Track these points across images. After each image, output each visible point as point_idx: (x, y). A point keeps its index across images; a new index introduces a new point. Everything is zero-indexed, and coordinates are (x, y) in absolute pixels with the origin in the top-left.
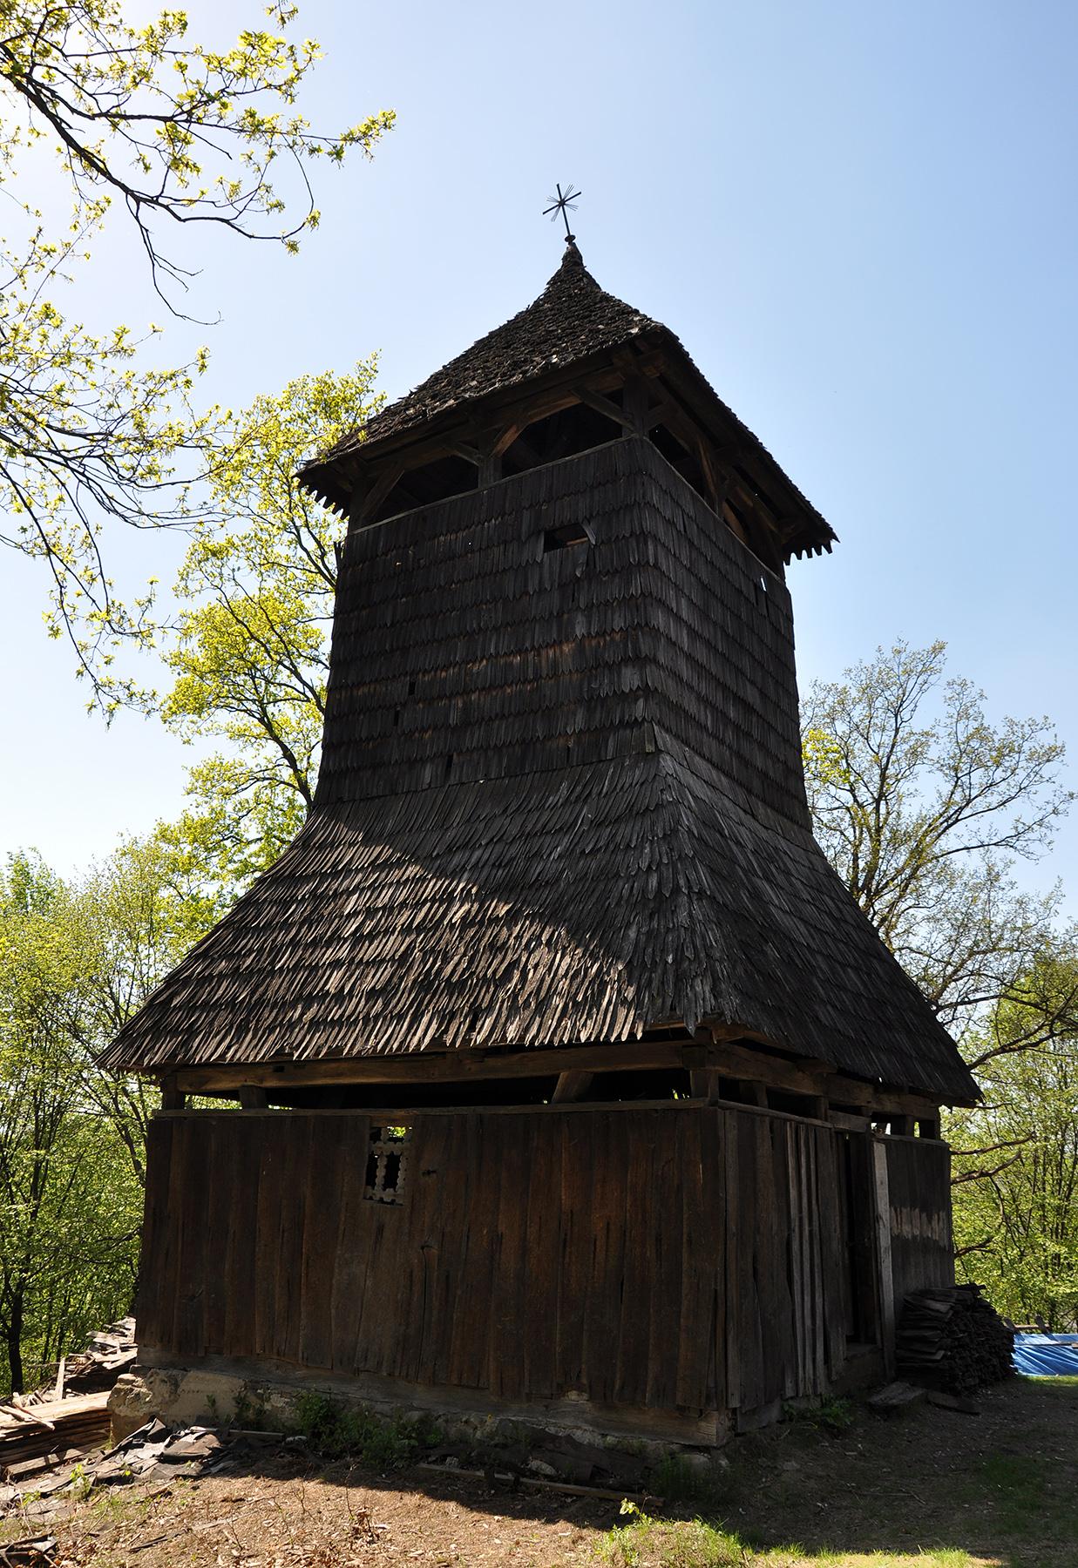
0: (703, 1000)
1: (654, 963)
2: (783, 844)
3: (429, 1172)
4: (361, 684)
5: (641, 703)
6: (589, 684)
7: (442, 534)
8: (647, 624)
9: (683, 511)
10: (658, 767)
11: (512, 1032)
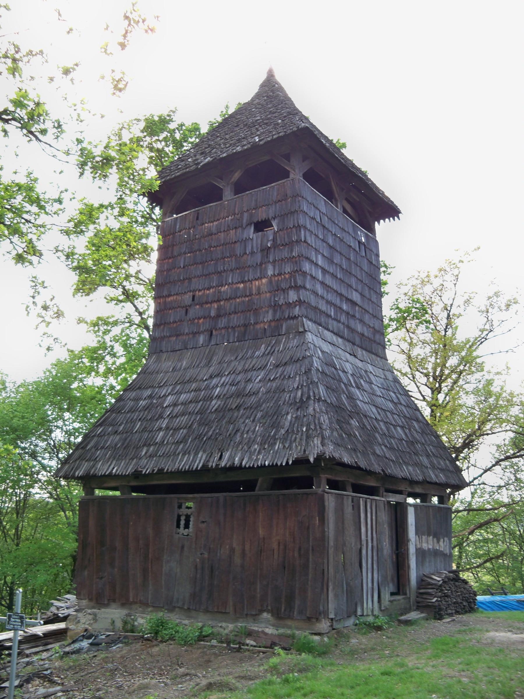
0: (317, 447)
1: (298, 431)
2: (370, 368)
3: (203, 522)
4: (169, 295)
5: (297, 308)
6: (274, 298)
7: (206, 223)
8: (300, 270)
9: (320, 211)
10: (304, 339)
11: (237, 460)
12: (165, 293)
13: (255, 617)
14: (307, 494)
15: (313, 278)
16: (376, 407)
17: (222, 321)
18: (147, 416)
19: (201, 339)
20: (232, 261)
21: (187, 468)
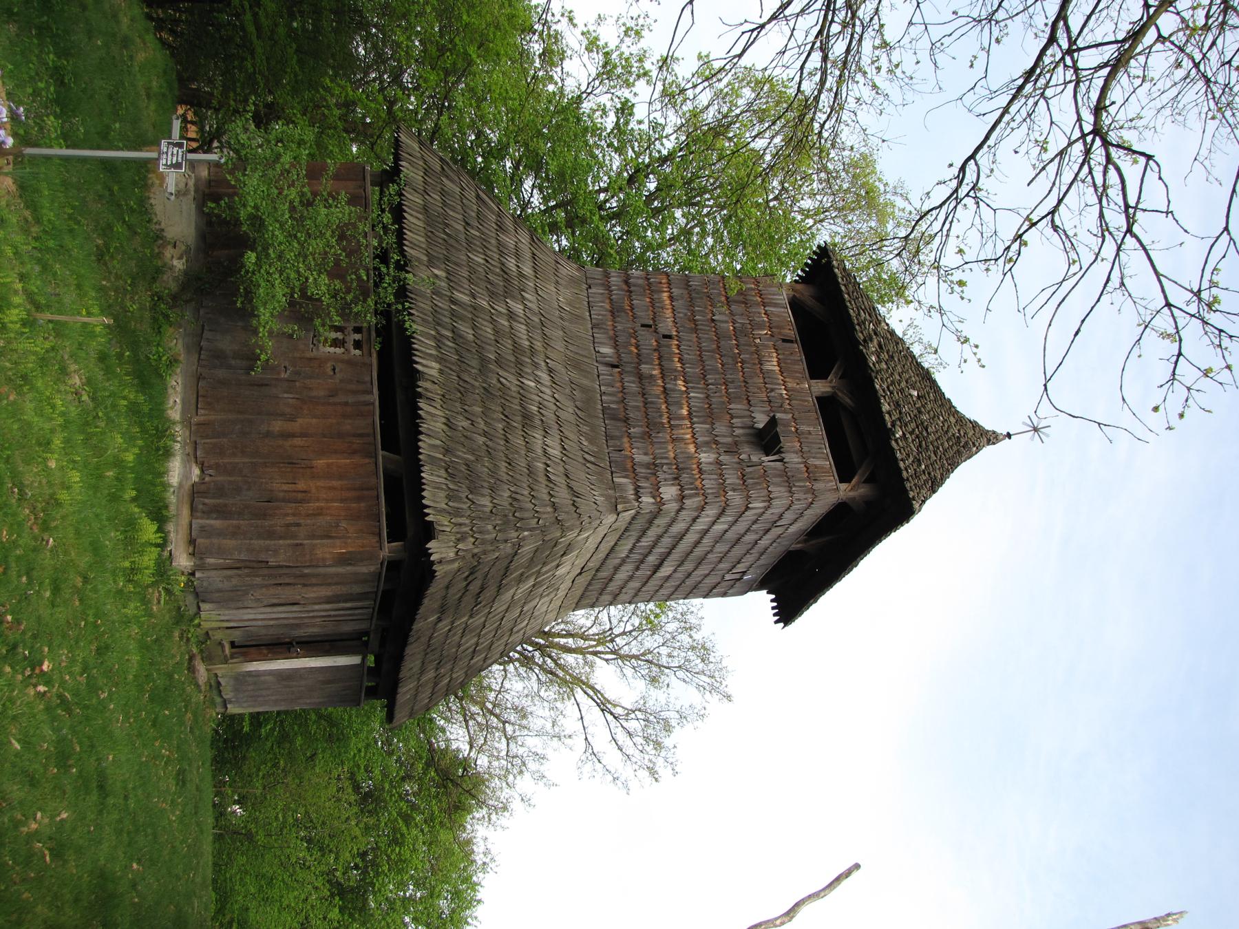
2: (561, 593)
5: (652, 500)
6: (667, 464)
12: (676, 291)
13: (193, 456)
14: (380, 535)
17: (633, 382)
19: (606, 350)
20: (720, 397)
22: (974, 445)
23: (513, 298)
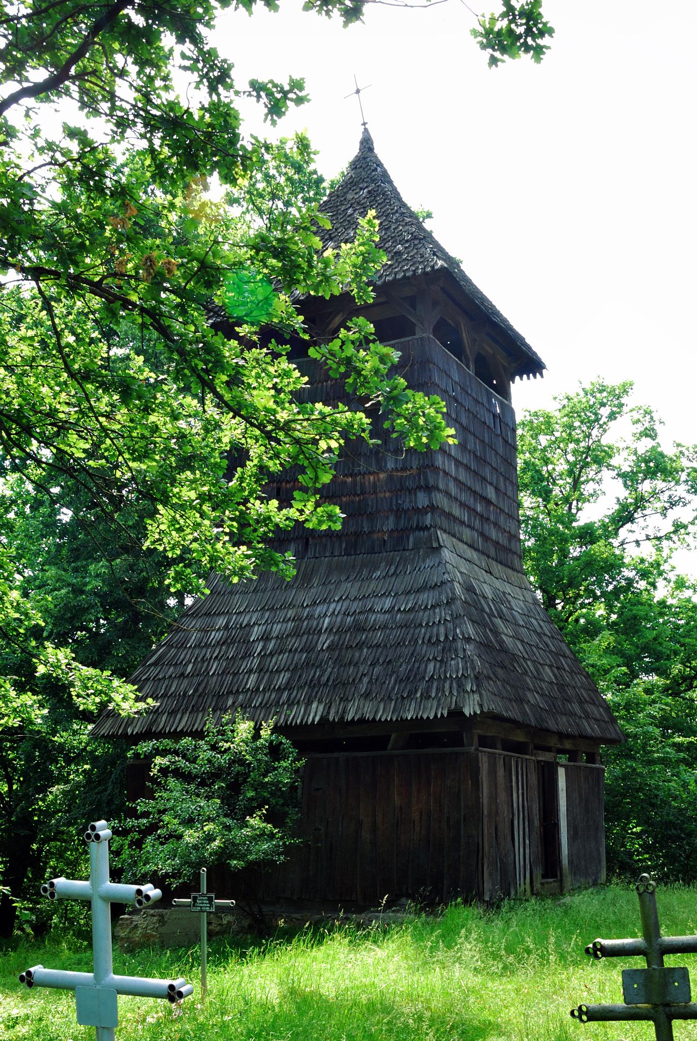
2: (508, 589)
6: (397, 500)
15: (446, 474)
16: (522, 641)
18: (226, 652)
21: (298, 722)
22: (376, 170)
23: (249, 634)
